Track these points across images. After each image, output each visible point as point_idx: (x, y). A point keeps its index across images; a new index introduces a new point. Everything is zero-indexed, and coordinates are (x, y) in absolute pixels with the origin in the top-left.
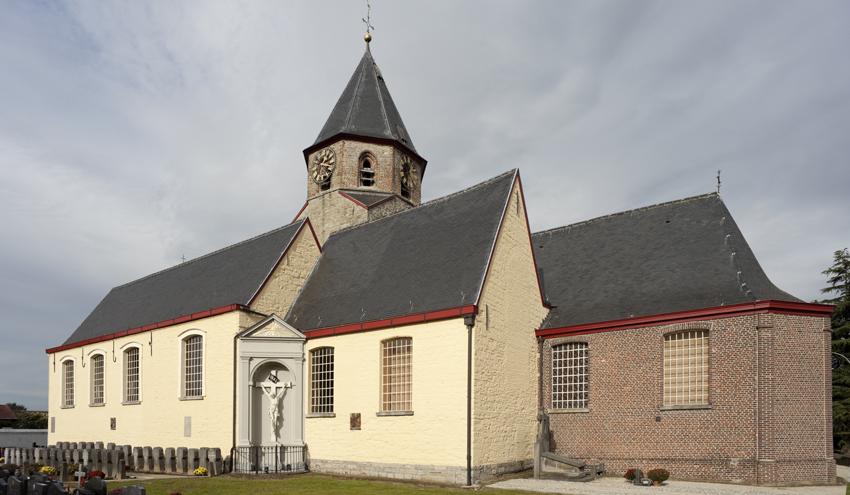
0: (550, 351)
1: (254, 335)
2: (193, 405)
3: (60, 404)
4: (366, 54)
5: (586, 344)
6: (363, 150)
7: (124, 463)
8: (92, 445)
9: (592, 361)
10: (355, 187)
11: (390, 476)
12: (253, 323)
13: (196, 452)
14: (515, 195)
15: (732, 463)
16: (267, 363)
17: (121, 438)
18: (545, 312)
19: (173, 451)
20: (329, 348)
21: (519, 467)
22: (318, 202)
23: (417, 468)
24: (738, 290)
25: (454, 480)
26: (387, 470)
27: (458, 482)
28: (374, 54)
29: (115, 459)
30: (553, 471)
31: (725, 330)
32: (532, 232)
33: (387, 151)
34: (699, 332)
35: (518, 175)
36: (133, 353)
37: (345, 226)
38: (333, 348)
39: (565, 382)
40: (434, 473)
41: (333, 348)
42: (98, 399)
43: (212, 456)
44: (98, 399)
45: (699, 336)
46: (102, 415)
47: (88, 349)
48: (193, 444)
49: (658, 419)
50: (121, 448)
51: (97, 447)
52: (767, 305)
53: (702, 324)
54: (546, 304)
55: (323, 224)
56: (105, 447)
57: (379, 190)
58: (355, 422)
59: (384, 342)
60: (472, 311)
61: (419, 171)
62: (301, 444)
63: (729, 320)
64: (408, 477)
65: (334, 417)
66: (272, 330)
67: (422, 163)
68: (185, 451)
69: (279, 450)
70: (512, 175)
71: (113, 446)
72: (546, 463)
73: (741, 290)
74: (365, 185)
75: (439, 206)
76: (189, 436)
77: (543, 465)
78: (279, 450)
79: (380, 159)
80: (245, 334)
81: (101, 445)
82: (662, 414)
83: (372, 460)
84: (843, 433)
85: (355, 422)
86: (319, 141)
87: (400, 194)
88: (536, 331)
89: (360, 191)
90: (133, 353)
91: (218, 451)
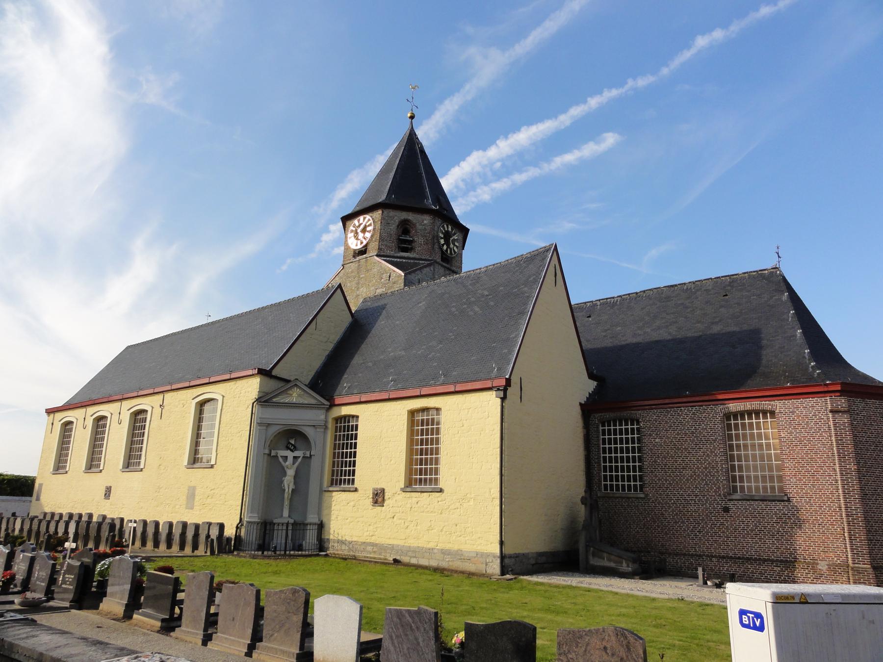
0: (598, 427)
1: (274, 400)
2: (198, 475)
3: (52, 470)
4: (411, 131)
5: (638, 423)
6: (403, 218)
7: (114, 536)
8: (80, 516)
9: (646, 440)
10: (392, 253)
11: (414, 561)
12: (280, 386)
13: (197, 527)
14: (551, 269)
15: (820, 567)
16: (285, 430)
17: (112, 510)
18: (592, 385)
19: (171, 525)
20: (353, 416)
21: (587, 590)
22: (353, 266)
23: (444, 552)
24: (807, 369)
25: (481, 568)
26: (410, 554)
27: (490, 571)
28: (420, 133)
29: (105, 533)
30: (602, 564)
31: (793, 412)
32: (573, 303)
33: (427, 220)
34: (765, 413)
35: (556, 249)
36: (138, 417)
37: (379, 291)
38: (357, 417)
39: (616, 462)
40: (463, 560)
41: (357, 417)
42: (93, 463)
43: (214, 533)
44: (93, 463)
45: (765, 417)
46: (98, 482)
47: (91, 410)
48: (193, 518)
49: (726, 510)
50: (113, 520)
51: (85, 519)
52: (839, 388)
53: (766, 405)
54: (591, 376)
55: (358, 289)
56: (95, 519)
57: (417, 256)
58: (379, 498)
59: (412, 413)
60: (503, 383)
61: (461, 238)
62: (316, 521)
63: (797, 402)
64: (434, 563)
65: (356, 490)
66: (295, 396)
67: (465, 231)
68: (185, 525)
69: (290, 527)
70: (550, 249)
71: (104, 517)
72: (594, 555)
73: (811, 370)
74: (403, 251)
75: (477, 277)
76: (192, 508)
77: (591, 558)
78: (290, 527)
79: (419, 227)
80: (264, 400)
81: (90, 516)
82: (730, 505)
83: (395, 542)
84: (842, 499)
85: (379, 498)
86: (358, 209)
87: (439, 260)
88: (581, 404)
89: (397, 257)
90: (138, 417)
91: (222, 527)
